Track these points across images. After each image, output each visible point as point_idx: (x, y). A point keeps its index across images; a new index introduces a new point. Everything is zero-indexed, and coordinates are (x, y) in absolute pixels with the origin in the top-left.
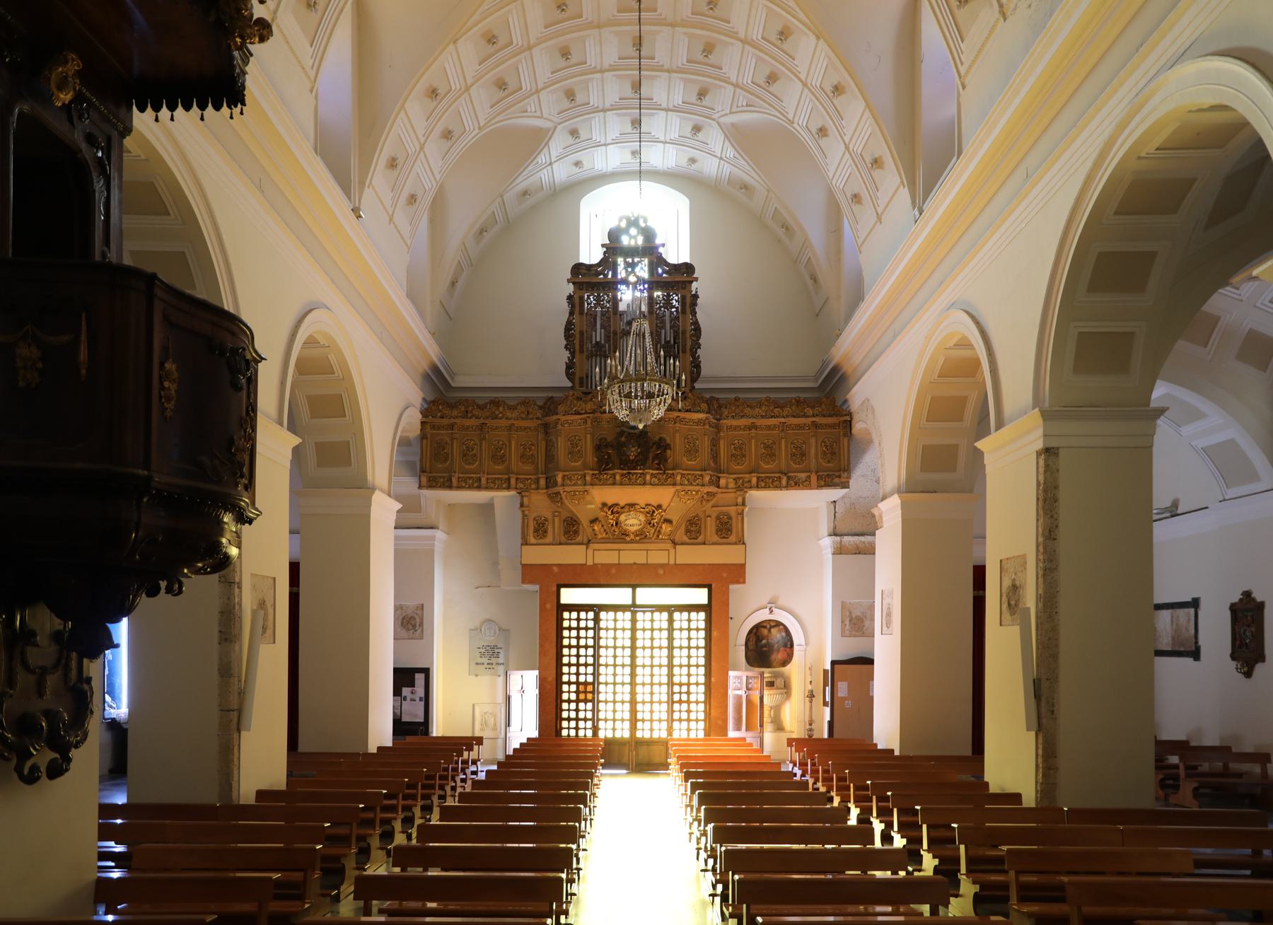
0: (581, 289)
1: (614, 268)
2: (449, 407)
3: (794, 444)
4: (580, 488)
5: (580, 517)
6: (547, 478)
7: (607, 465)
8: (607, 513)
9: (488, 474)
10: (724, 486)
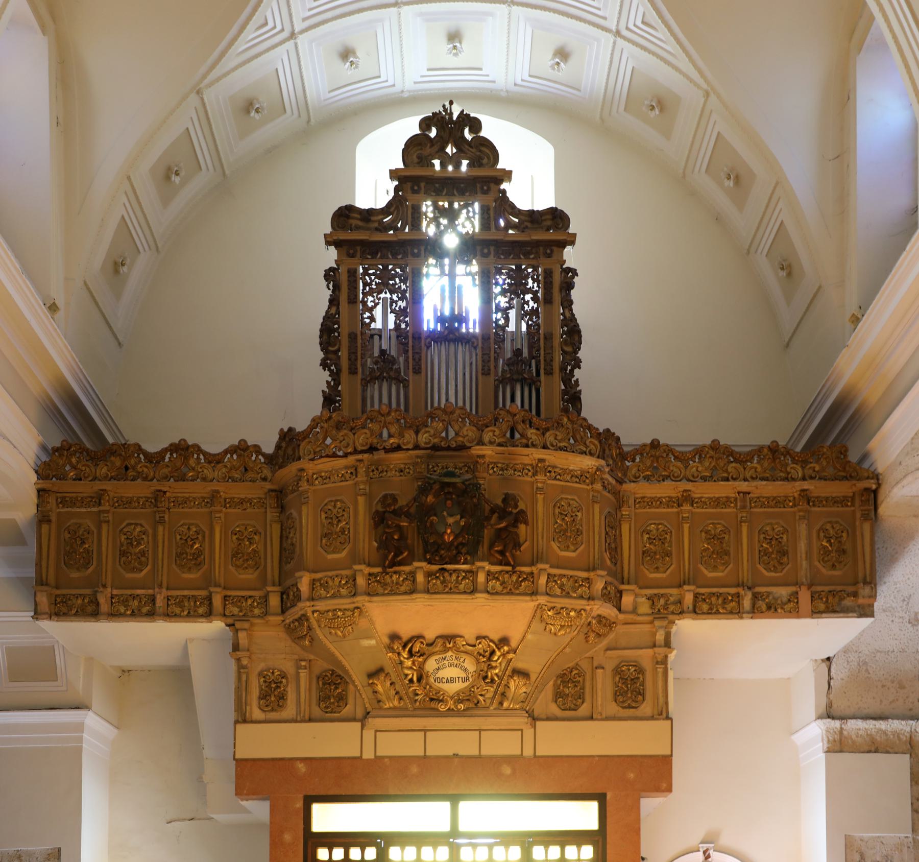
0: (352, 256)
1: (416, 218)
2: (92, 459)
3: (766, 532)
4: (344, 603)
5: (348, 667)
6: (282, 594)
7: (398, 553)
8: (399, 654)
9: (168, 589)
10: (630, 608)
